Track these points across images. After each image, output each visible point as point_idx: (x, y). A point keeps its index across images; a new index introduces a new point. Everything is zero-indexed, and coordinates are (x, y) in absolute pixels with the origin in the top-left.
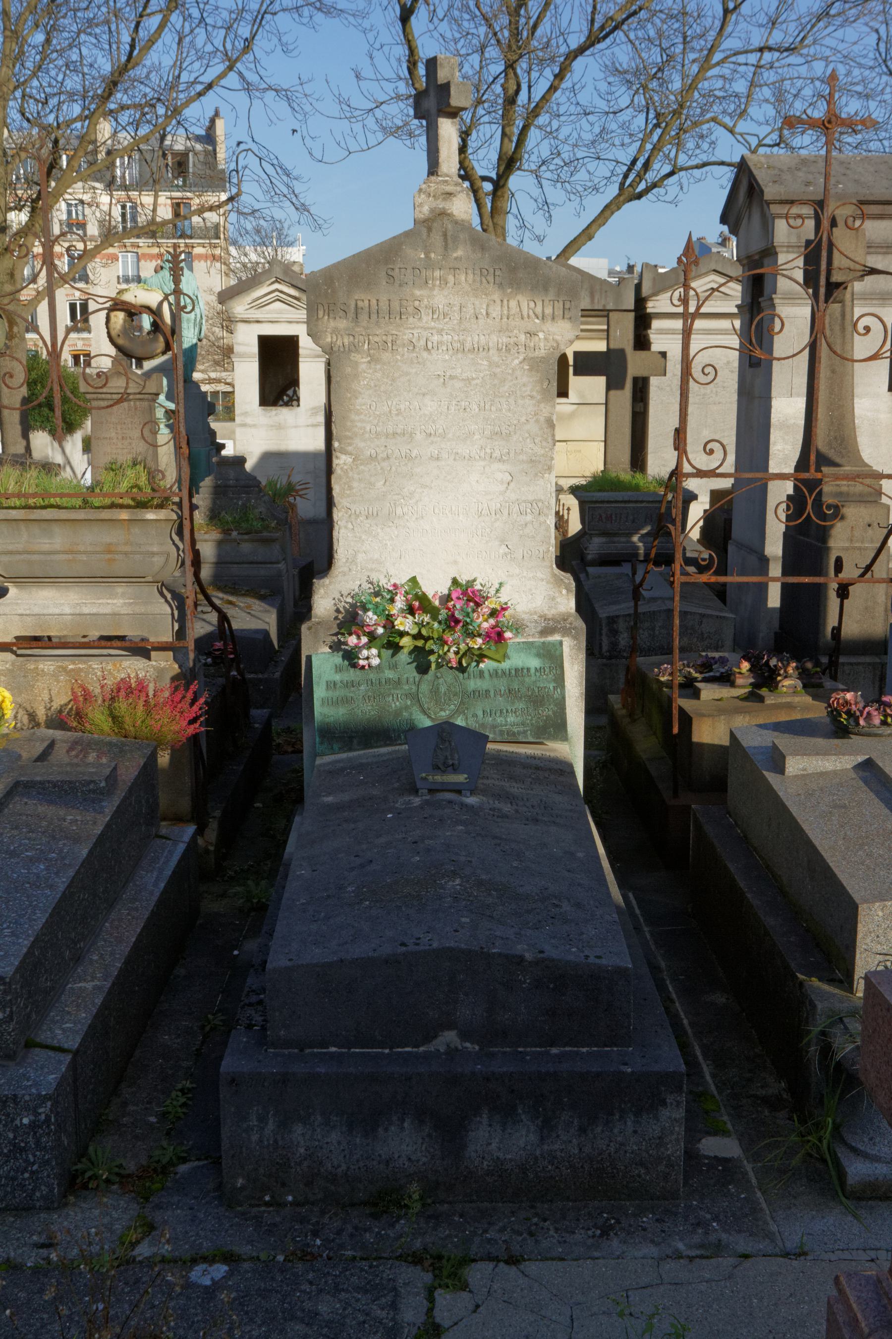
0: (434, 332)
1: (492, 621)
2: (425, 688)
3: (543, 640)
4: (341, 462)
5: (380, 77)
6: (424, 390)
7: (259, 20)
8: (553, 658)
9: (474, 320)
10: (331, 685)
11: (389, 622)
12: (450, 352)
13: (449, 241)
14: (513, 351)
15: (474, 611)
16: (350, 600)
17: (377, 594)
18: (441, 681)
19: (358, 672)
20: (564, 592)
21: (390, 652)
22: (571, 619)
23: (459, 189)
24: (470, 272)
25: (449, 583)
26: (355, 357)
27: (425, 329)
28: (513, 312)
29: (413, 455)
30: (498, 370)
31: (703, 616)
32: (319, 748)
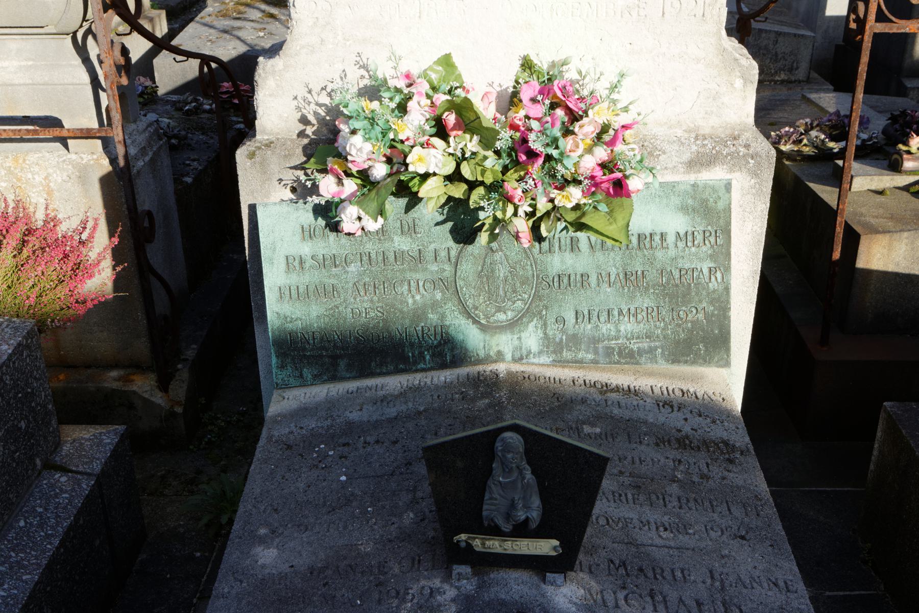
2: (468, 268)
3: (692, 178)
8: (711, 214)
10: (295, 264)
11: (396, 157)
15: (567, 132)
16: (326, 100)
17: (372, 92)
18: (498, 256)
19: (344, 240)
20: (739, 83)
21: (403, 202)
31: (779, 34)
32: (279, 375)
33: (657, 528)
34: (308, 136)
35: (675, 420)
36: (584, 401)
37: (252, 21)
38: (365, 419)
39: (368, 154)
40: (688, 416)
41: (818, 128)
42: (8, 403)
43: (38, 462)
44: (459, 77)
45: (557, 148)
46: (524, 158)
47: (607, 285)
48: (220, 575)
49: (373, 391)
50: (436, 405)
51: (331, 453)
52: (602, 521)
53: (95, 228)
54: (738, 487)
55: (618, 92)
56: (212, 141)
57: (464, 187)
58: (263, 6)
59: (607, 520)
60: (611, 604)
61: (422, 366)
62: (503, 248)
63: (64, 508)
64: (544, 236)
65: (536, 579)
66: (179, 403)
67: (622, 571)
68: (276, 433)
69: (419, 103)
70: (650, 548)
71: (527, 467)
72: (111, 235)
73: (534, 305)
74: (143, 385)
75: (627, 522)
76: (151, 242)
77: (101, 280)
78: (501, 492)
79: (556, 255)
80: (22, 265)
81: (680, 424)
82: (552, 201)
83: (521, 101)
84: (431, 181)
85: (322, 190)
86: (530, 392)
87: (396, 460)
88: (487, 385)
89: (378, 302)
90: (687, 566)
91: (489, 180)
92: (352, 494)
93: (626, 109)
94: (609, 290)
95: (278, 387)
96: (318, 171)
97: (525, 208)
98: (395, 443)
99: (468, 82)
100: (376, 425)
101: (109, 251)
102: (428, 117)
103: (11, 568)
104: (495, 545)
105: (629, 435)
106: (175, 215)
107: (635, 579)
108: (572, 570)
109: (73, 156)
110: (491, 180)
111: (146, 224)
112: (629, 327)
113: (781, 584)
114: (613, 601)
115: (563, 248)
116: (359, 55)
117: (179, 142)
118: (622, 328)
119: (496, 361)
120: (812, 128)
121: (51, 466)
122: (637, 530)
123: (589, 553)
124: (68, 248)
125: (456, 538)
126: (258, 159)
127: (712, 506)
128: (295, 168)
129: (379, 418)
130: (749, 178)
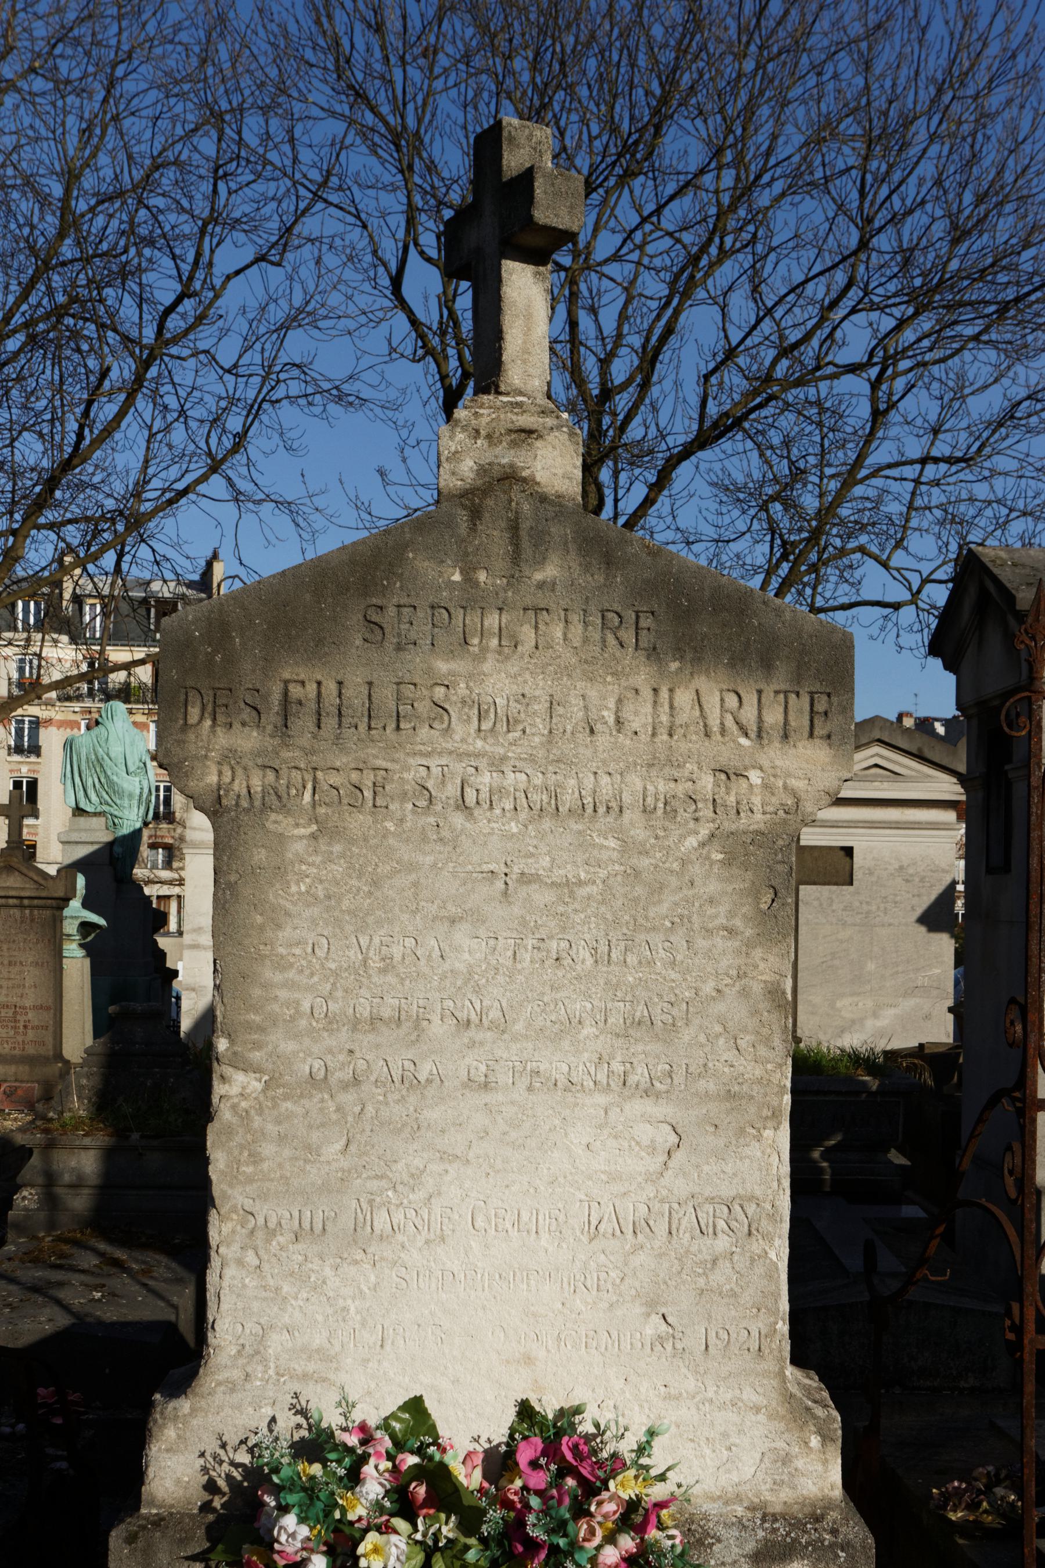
0: (483, 763)
1: (627, 1543)
4: (234, 1090)
5: (414, 482)
6: (453, 909)
7: (254, 410)
9: (583, 737)
12: (523, 815)
13: (526, 544)
14: (683, 816)
16: (243, 1458)
20: (815, 1441)
22: (834, 1515)
23: (550, 421)
24: (575, 618)
25: (510, 1415)
26: (277, 822)
27: (460, 756)
28: (682, 718)
29: (422, 1078)
30: (645, 862)
34: (214, 1510)
37: (83, 1271)
39: (302, 1541)
44: (432, 1430)
45: (565, 1535)
46: (520, 1548)
55: (649, 1456)
58: (102, 1246)
69: (376, 1467)
83: (517, 1464)
93: (662, 1478)
99: (444, 1431)
102: (388, 1487)
116: (296, 1396)
120: (998, 1483)
126: (140, 1544)
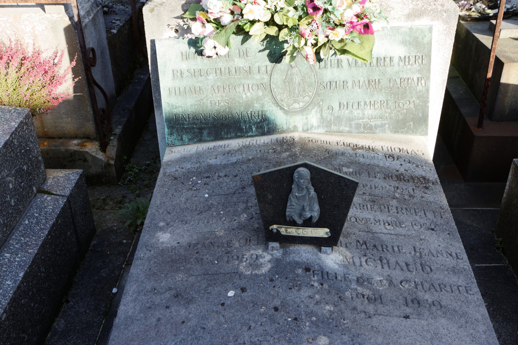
3: (409, 24)
10: (178, 74)
18: (295, 70)
21: (240, 38)
32: (169, 139)
33: (384, 224)
35: (395, 165)
36: (343, 154)
38: (219, 163)
40: (403, 163)
41: (481, 2)
42: (17, 155)
43: (34, 189)
45: (331, 4)
47: (358, 88)
48: (138, 248)
49: (223, 148)
50: (259, 156)
51: (199, 182)
52: (353, 220)
53: (62, 56)
54: (430, 202)
56: (127, 9)
57: (276, 29)
59: (356, 219)
60: (358, 264)
61: (251, 134)
62: (298, 66)
63: (50, 214)
64: (322, 58)
65: (315, 250)
66: (112, 159)
67: (364, 246)
68: (168, 171)
70: (380, 235)
71: (312, 187)
72: (71, 60)
73: (315, 99)
74: (92, 148)
75: (367, 220)
76: (94, 66)
77: (66, 87)
78: (297, 202)
79: (329, 70)
80: (21, 77)
81: (398, 168)
82: (327, 37)
84: (257, 25)
85: (193, 31)
86: (312, 149)
87: (236, 185)
88: (288, 145)
89: (226, 97)
90: (401, 245)
91: (290, 25)
92: (212, 204)
94: (359, 90)
95: (168, 145)
96: (191, 19)
97: (311, 41)
98: (236, 176)
100: (225, 166)
101: (70, 70)
103: (22, 246)
104: (293, 231)
105: (369, 173)
106: (108, 52)
107: (371, 251)
108: (336, 245)
109: (47, 15)
110: (292, 25)
111: (91, 55)
112: (370, 112)
113: (454, 255)
114: (359, 263)
115: (333, 65)
117: (109, 10)
118: (366, 113)
119: (293, 132)
121: (41, 191)
122: (373, 225)
123: (346, 237)
124: (47, 68)
125: (271, 227)
126: (155, 12)
127: (416, 212)
128: (177, 18)
129: (226, 163)
130: (443, 24)
